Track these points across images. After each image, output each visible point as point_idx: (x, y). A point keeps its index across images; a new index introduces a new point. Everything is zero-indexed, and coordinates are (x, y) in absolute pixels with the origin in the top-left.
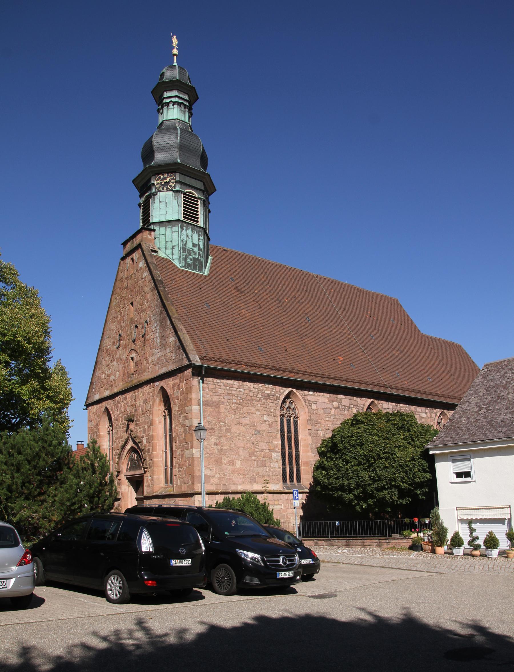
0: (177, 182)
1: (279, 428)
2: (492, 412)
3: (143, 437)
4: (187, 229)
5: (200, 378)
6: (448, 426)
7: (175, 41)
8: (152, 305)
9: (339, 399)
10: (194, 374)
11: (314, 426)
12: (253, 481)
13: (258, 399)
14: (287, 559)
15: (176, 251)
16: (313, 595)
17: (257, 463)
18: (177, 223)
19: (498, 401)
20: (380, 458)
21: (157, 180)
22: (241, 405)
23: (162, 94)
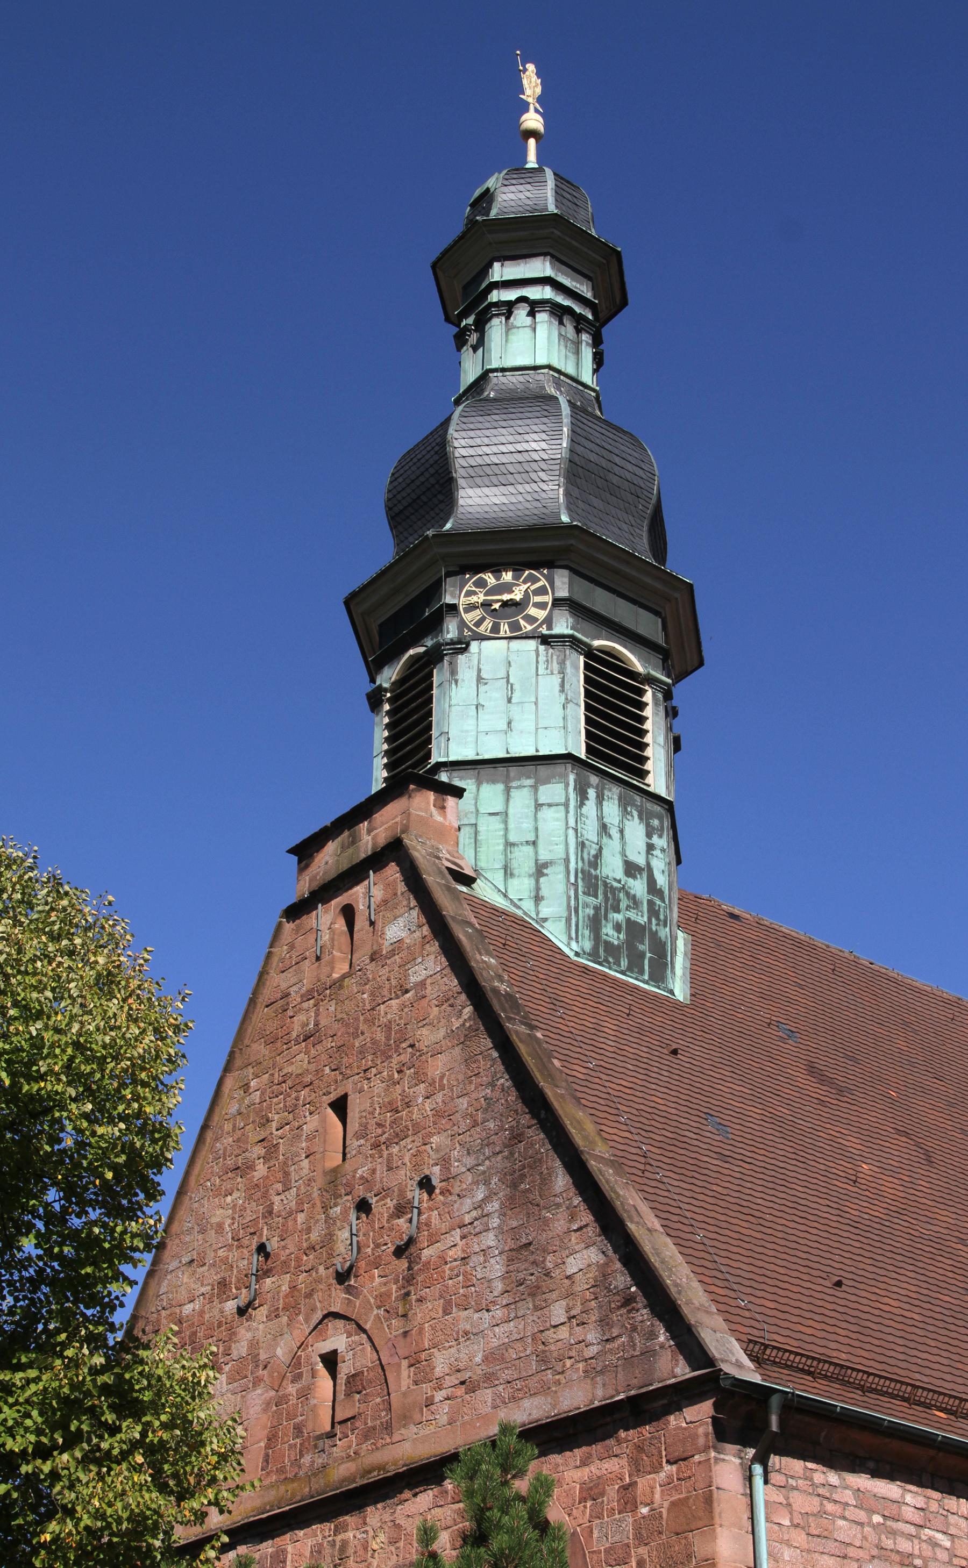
0: (557, 602)
4: (600, 799)
5: (751, 1452)
7: (532, 84)
8: (463, 1103)
10: (724, 1432)
15: (556, 885)
18: (559, 768)
21: (469, 594)
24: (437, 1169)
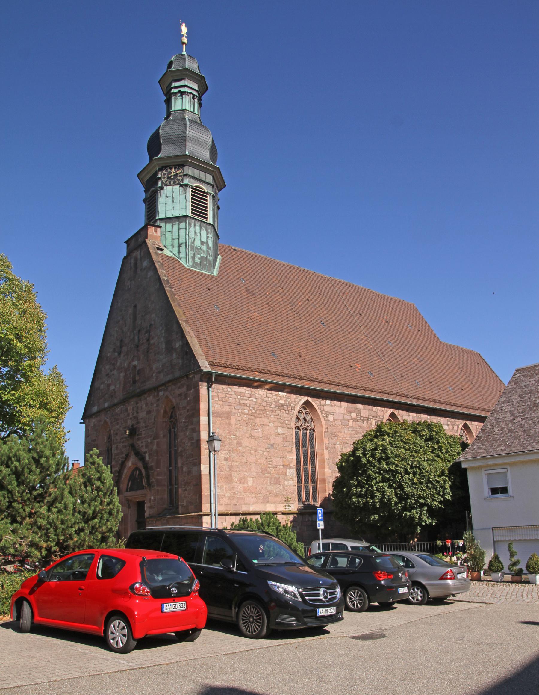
1: (294, 441)
2: (529, 420)
3: (145, 452)
4: (195, 226)
6: (481, 437)
7: (184, 30)
9: (356, 410)
11: (331, 439)
12: (266, 500)
14: (328, 591)
16: (357, 635)
17: (270, 481)
19: (535, 408)
20: (407, 472)
22: (254, 416)
23: (171, 83)
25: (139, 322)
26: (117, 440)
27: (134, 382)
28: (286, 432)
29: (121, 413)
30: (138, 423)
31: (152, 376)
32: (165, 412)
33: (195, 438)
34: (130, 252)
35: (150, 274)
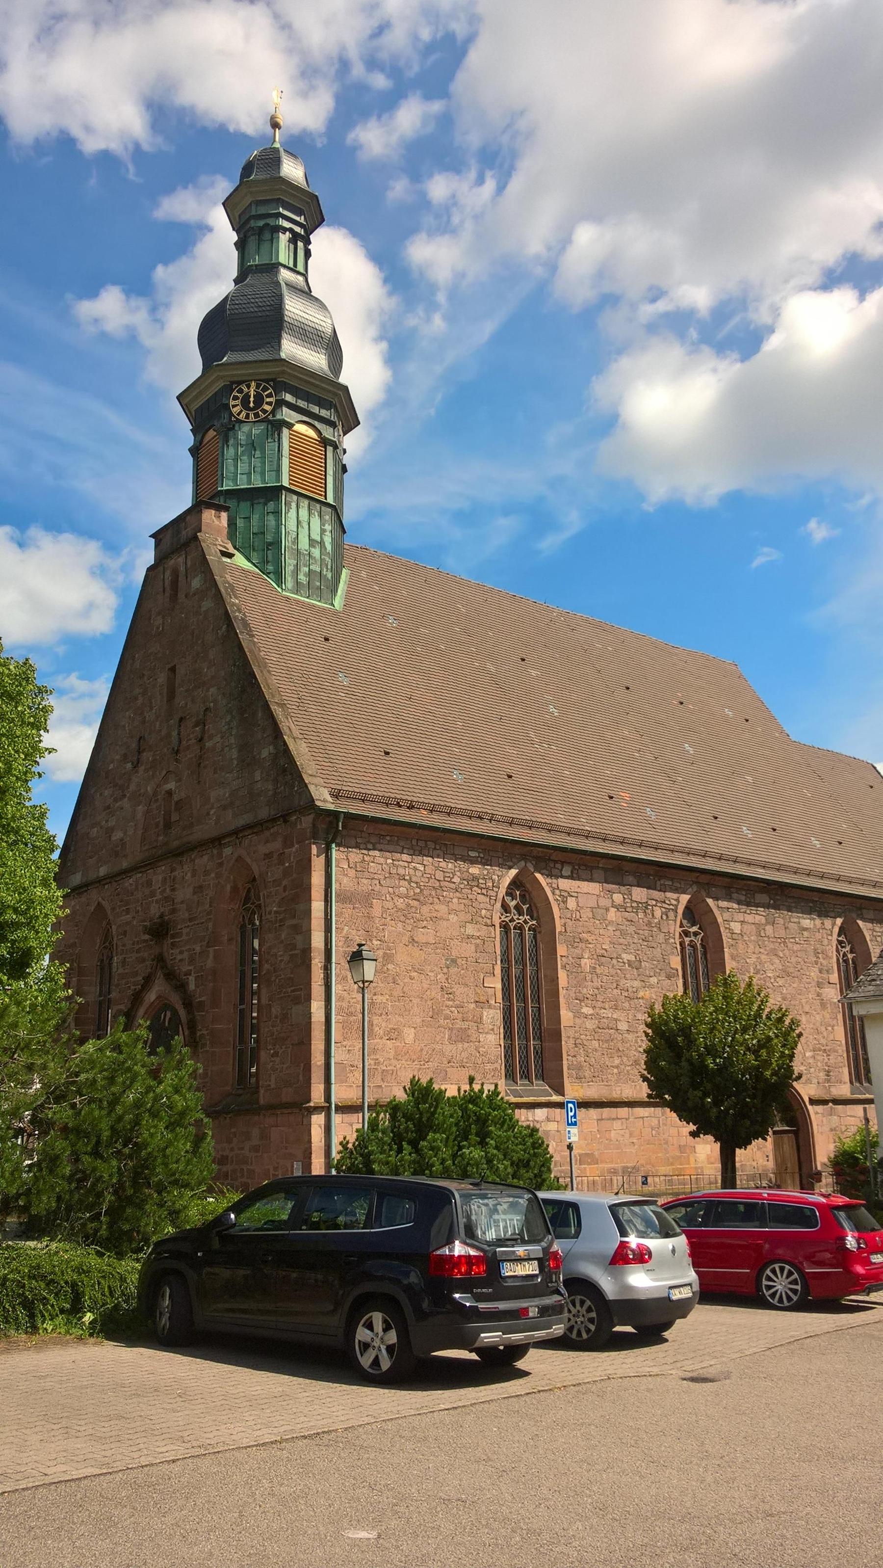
3: (188, 973)
13: (453, 886)
24: (212, 704)
25: (180, 701)
26: (124, 945)
27: (168, 825)
28: (484, 932)
29: (137, 889)
30: (174, 911)
31: (208, 814)
32: (235, 889)
33: (300, 945)
34: (160, 559)
35: (207, 604)
